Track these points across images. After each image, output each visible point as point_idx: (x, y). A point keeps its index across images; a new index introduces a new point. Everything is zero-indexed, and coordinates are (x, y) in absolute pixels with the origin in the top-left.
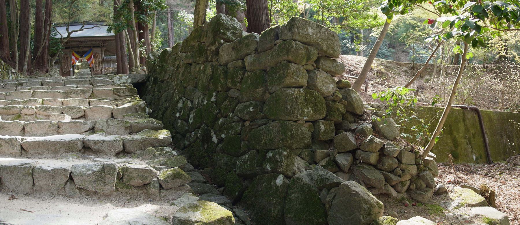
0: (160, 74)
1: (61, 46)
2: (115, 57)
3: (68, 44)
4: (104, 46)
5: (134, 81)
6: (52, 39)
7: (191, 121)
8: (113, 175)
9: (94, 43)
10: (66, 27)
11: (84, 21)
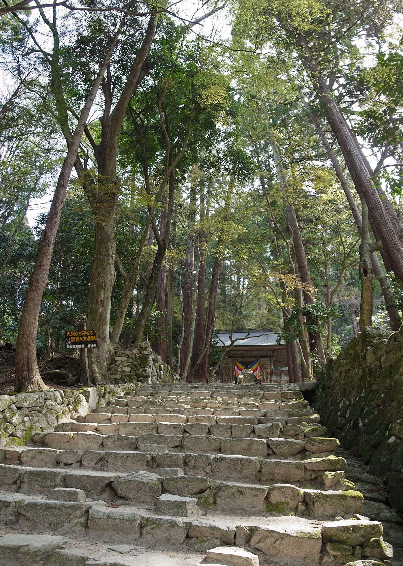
0: (327, 381)
1: (223, 354)
2: (287, 369)
3: (231, 353)
4: (273, 356)
5: (303, 389)
6: (212, 346)
7: (347, 416)
8: (278, 428)
9: (261, 352)
10: (228, 335)
11: (250, 329)
